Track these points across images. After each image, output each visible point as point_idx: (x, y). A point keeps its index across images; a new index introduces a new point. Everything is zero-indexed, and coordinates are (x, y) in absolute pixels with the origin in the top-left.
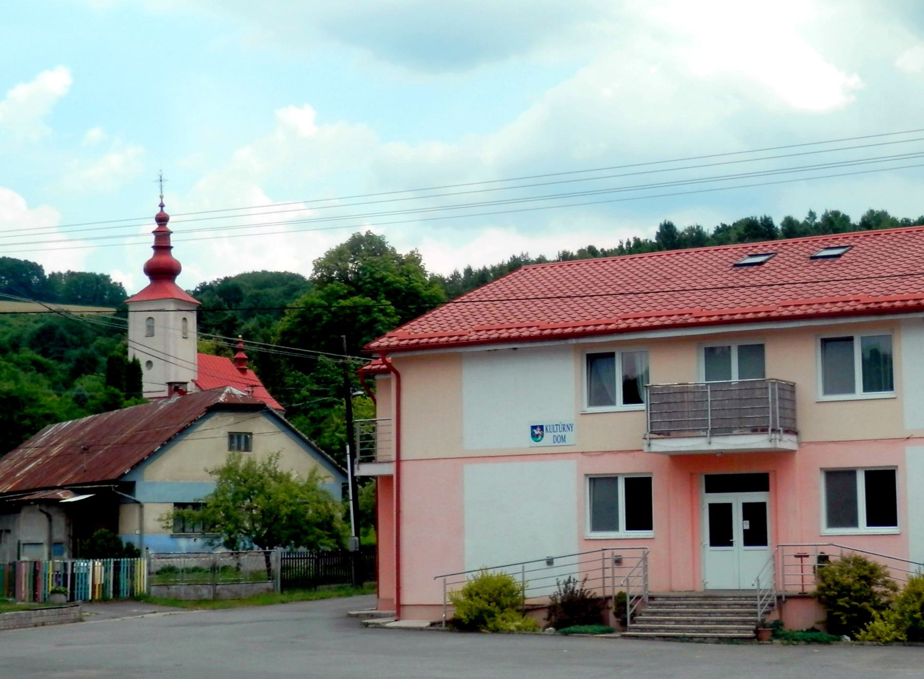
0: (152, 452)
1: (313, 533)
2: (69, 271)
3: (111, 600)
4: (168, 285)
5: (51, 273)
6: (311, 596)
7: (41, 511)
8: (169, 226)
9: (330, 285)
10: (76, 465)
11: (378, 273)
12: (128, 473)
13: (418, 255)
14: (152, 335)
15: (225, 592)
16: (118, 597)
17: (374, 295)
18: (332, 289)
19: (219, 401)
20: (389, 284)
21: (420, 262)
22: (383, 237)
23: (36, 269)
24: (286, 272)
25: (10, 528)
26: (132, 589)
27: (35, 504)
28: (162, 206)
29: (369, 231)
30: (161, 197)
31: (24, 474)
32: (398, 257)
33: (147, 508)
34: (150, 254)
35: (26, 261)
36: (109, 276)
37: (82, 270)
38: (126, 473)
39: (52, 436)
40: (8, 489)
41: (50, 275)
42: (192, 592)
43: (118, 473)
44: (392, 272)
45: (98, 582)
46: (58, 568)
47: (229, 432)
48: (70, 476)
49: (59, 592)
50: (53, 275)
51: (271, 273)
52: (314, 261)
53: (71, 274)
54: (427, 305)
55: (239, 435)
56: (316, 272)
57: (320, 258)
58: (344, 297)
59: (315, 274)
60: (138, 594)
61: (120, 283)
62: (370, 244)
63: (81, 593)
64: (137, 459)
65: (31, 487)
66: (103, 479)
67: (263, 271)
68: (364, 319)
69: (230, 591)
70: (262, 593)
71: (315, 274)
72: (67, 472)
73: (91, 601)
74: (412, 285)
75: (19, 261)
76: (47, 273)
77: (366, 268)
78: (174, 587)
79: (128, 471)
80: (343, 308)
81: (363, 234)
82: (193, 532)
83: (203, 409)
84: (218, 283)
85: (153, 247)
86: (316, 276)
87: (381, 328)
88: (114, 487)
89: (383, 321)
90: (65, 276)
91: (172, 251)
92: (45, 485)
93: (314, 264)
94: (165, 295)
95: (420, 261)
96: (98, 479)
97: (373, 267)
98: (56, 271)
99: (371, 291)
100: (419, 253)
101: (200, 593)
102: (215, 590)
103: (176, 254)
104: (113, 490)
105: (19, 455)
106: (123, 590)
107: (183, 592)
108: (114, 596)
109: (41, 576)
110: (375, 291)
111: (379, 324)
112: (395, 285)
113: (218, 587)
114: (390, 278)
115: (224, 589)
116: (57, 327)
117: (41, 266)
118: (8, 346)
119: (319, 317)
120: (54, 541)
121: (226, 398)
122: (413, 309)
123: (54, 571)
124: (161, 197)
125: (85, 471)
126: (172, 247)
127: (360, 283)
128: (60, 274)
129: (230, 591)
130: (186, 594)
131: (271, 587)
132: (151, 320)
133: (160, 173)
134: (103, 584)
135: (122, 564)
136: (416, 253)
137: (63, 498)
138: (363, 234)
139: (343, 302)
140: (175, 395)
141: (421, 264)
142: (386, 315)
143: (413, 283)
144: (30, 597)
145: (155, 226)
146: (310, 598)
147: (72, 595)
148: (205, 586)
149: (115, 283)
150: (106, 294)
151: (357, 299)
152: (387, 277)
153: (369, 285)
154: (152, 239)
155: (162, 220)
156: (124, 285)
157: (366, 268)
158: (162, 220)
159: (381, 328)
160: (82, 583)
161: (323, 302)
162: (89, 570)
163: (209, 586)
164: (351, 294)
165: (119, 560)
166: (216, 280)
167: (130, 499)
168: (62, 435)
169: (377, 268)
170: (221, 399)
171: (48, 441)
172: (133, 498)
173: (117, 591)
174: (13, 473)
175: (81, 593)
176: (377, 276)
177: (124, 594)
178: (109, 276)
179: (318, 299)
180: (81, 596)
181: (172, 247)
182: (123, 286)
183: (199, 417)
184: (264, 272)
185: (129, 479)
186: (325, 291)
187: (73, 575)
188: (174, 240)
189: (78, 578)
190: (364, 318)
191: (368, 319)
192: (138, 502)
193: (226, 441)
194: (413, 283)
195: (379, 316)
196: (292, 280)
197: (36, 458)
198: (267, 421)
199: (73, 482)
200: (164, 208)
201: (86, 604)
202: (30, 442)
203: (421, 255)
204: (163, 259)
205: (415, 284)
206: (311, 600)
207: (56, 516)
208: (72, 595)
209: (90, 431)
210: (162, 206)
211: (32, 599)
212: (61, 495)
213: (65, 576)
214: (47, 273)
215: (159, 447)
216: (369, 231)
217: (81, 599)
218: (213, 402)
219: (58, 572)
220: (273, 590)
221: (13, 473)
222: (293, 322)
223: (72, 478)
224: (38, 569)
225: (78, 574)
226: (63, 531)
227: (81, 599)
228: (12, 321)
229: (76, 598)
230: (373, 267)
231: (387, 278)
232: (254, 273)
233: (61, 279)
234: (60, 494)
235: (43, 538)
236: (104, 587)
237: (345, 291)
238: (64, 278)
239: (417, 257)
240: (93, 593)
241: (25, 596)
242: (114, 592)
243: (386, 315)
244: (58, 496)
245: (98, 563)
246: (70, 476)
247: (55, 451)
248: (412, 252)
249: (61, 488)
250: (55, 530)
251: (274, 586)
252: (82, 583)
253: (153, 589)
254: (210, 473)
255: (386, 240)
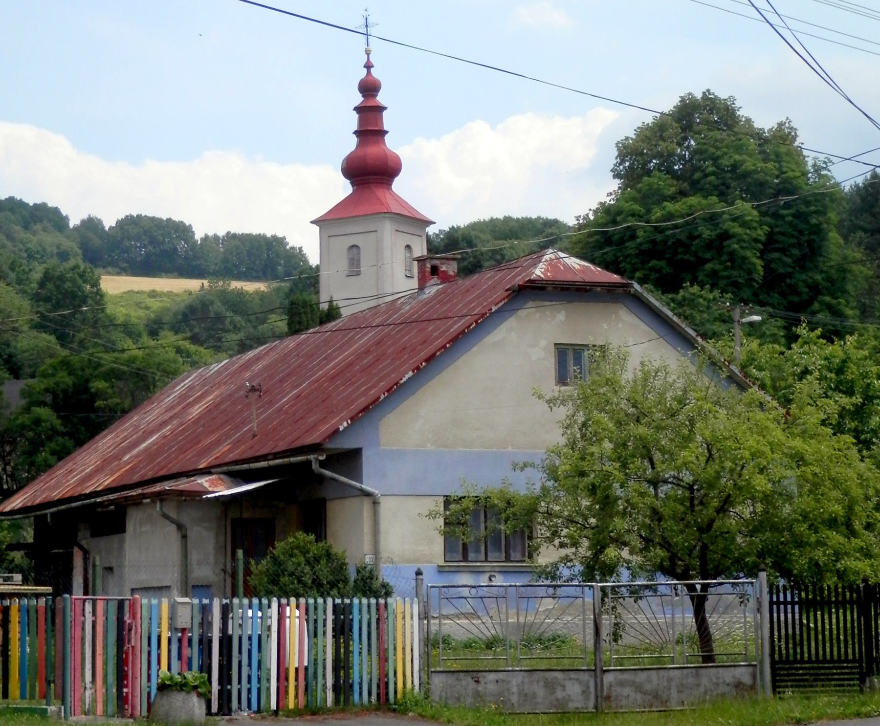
0: (396, 384)
1: (820, 543)
2: (228, 233)
3: (329, 711)
4: (380, 192)
5: (203, 236)
6: (864, 704)
7: (165, 516)
8: (382, 98)
9: (646, 179)
10: (237, 428)
11: (726, 157)
12: (345, 429)
13: (792, 128)
14: (358, 274)
15: (626, 691)
16: (347, 701)
17: (723, 195)
18: (650, 185)
19: (533, 277)
20: (746, 175)
21: (795, 140)
22: (732, 99)
23: (183, 230)
24: (539, 218)
25: (114, 564)
26: (383, 685)
27: (153, 502)
28: (368, 66)
29: (708, 91)
30: (368, 53)
31: (137, 456)
32: (758, 135)
33: (387, 506)
34: (351, 144)
35: (169, 220)
36: (284, 238)
37: (247, 231)
38: (341, 428)
39: (191, 388)
40: (106, 483)
41: (201, 239)
42: (540, 692)
43: (325, 429)
44: (750, 155)
45: (293, 663)
46: (184, 619)
47: (555, 344)
48: (224, 447)
49: (182, 687)
50: (206, 238)
51: (518, 219)
52: (619, 142)
53: (231, 237)
54: (813, 208)
55: (578, 350)
56: (622, 162)
57: (627, 138)
58: (673, 198)
59: (620, 164)
60: (408, 696)
61: (300, 249)
62: (711, 111)
63: (249, 691)
64: (363, 401)
65: (150, 475)
66: (291, 447)
67: (505, 217)
68: (707, 233)
69: (639, 688)
70: (723, 695)
71: (620, 164)
72: (218, 442)
73: (276, 713)
74: (785, 175)
75: (160, 220)
76: (198, 236)
77: (706, 151)
78: (492, 676)
79: (345, 424)
80: (670, 217)
81: (699, 96)
82: (486, 560)
83: (500, 293)
84: (442, 236)
85: (355, 133)
86: (621, 167)
87: (736, 246)
88: (316, 459)
89: (740, 235)
90: (223, 239)
91: (387, 137)
92: (174, 470)
93: (617, 146)
94: (378, 208)
95: (794, 138)
96: (282, 446)
97: (717, 148)
98: (211, 234)
99: (716, 187)
100: (792, 124)
101: (560, 694)
102: (599, 686)
103: (393, 143)
104: (314, 467)
105: (131, 425)
106: (361, 684)
107: (515, 690)
108: (337, 701)
109: (135, 640)
110: (722, 188)
111: (735, 240)
112: (755, 176)
113: (608, 678)
114: (747, 164)
115: (622, 684)
116: (212, 303)
117: (190, 225)
118: (141, 328)
119: (631, 234)
120: (191, 583)
121: (547, 270)
122: (788, 215)
123: (172, 628)
124: (368, 53)
125: (254, 436)
126: (386, 132)
127: (697, 175)
128: (216, 237)
129: (639, 688)
130: (525, 696)
131: (747, 680)
132: (355, 250)
133: (364, 13)
134: (306, 668)
135: (356, 611)
136: (787, 125)
137: (210, 489)
138: (699, 96)
139: (670, 206)
140: (432, 282)
141: (796, 144)
142: (745, 225)
143: (786, 173)
144: (106, 703)
145: (358, 99)
146: (863, 710)
147: (225, 696)
148: (573, 675)
149: (292, 248)
150: (280, 264)
151: (693, 200)
152: (744, 161)
153: (712, 178)
154: (353, 121)
155: (369, 88)
156: (305, 251)
157: (706, 151)
158: (369, 88)
159: (736, 246)
160: (250, 665)
161: (636, 207)
162: (269, 628)
163: (585, 677)
164: (683, 194)
165: (347, 601)
166: (437, 232)
167: (350, 486)
168: (208, 385)
169: (725, 150)
170: (539, 272)
171: (183, 397)
172: (358, 484)
173: (342, 688)
174: (117, 457)
175: (249, 691)
176: (725, 162)
177: (362, 696)
178: (284, 238)
179: (627, 202)
180: (249, 700)
181: (386, 132)
182: (305, 252)
183: (494, 309)
184: (507, 219)
185: (348, 444)
186: (639, 191)
187: (226, 641)
188: (388, 121)
189: (240, 652)
190: (708, 232)
191: (714, 234)
192: (368, 494)
193: (550, 364)
194: (786, 173)
195: (733, 227)
196: (550, 227)
197: (164, 424)
198: (637, 321)
199: (231, 457)
200: (372, 70)
201: (73, 455)
202: (153, 403)
203: (796, 129)
204: (372, 151)
205: (790, 174)
206: (868, 715)
207: (195, 528)
208: (225, 696)
209: (265, 368)
210: (368, 66)
211: (112, 707)
212: (206, 485)
213: (205, 644)
214: (198, 236)
215: (411, 374)
216: (708, 91)
217: (249, 707)
218: (519, 280)
219: (183, 630)
220: (752, 687)
221: (117, 457)
222: (588, 243)
223: (230, 451)
224: (127, 619)
225: (240, 638)
226: (211, 559)
227: (249, 707)
228: (150, 302)
229: (234, 704)
230: (717, 148)
231: (742, 165)
232: (492, 220)
233: (218, 245)
234: (204, 482)
235: (172, 577)
236: (309, 675)
237: (673, 189)
238: (222, 244)
239: (790, 133)
240: (282, 692)
241: (94, 700)
242: (336, 688)
243: (745, 225)
244: (201, 485)
245: (294, 613)
246: (224, 447)
247: (196, 411)
248: (781, 125)
249: (206, 471)
250: (194, 556)
251: (754, 677)
252: (250, 665)
253: (438, 681)
254: (549, 402)
255: (738, 104)
